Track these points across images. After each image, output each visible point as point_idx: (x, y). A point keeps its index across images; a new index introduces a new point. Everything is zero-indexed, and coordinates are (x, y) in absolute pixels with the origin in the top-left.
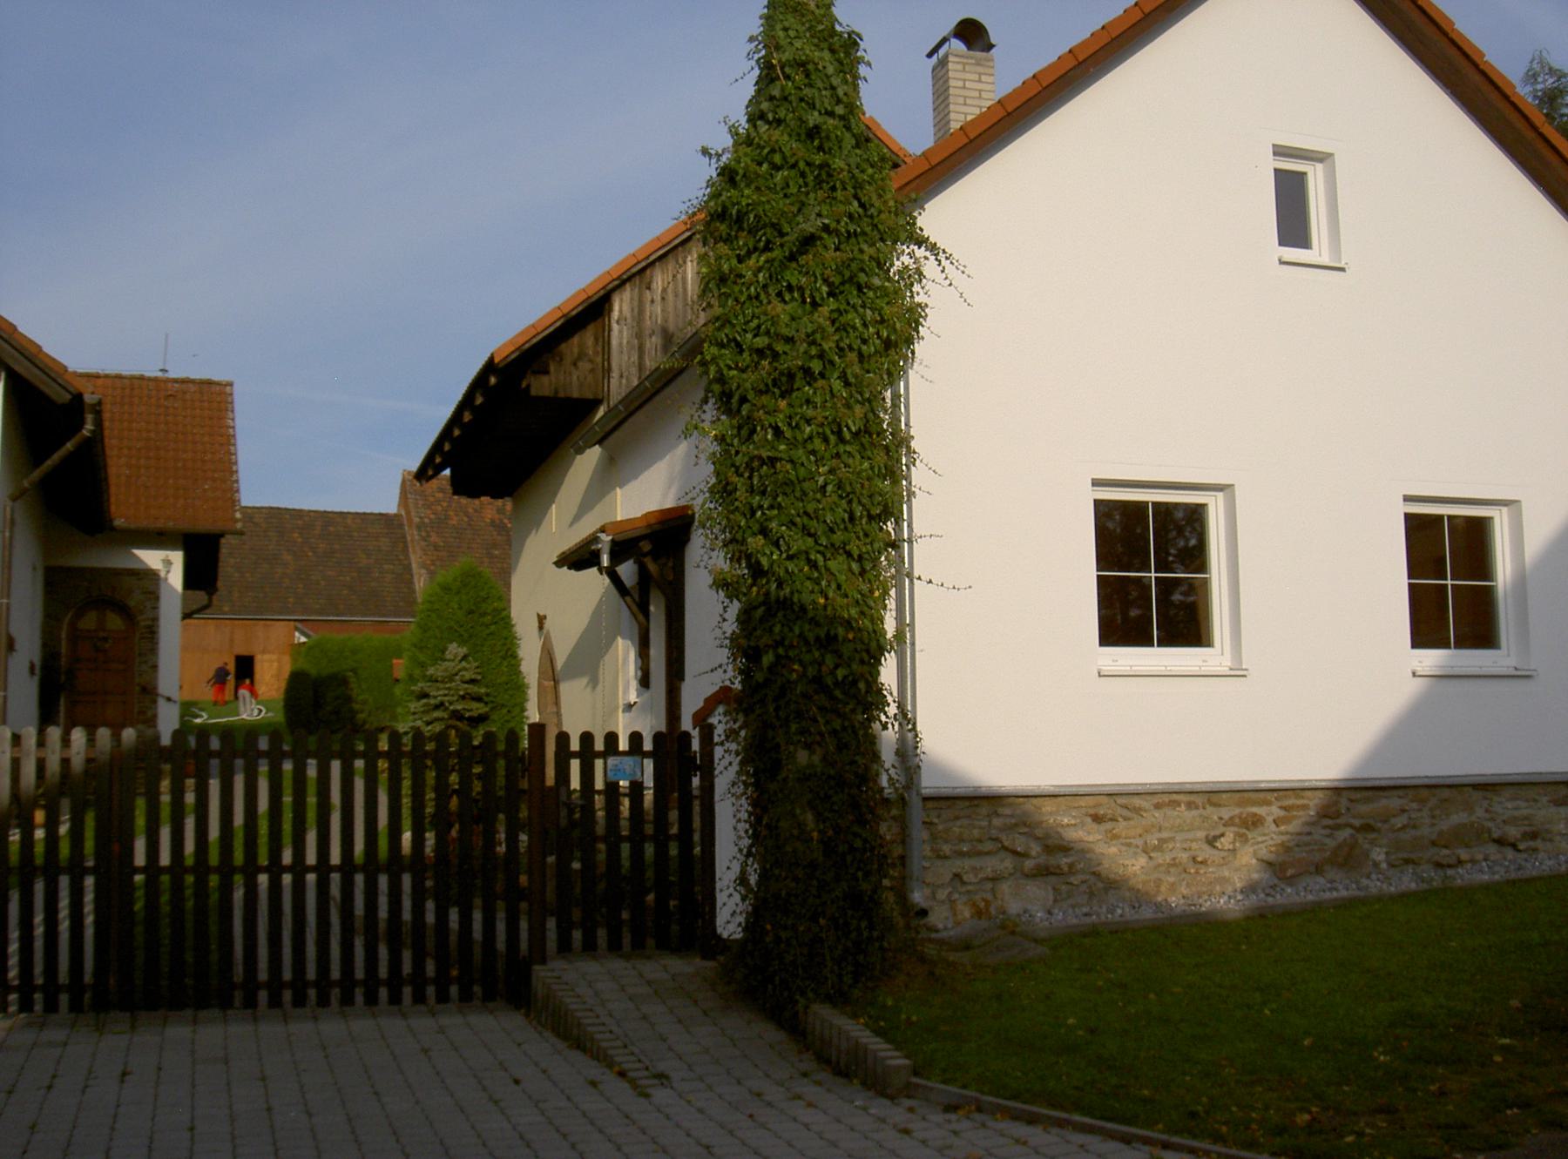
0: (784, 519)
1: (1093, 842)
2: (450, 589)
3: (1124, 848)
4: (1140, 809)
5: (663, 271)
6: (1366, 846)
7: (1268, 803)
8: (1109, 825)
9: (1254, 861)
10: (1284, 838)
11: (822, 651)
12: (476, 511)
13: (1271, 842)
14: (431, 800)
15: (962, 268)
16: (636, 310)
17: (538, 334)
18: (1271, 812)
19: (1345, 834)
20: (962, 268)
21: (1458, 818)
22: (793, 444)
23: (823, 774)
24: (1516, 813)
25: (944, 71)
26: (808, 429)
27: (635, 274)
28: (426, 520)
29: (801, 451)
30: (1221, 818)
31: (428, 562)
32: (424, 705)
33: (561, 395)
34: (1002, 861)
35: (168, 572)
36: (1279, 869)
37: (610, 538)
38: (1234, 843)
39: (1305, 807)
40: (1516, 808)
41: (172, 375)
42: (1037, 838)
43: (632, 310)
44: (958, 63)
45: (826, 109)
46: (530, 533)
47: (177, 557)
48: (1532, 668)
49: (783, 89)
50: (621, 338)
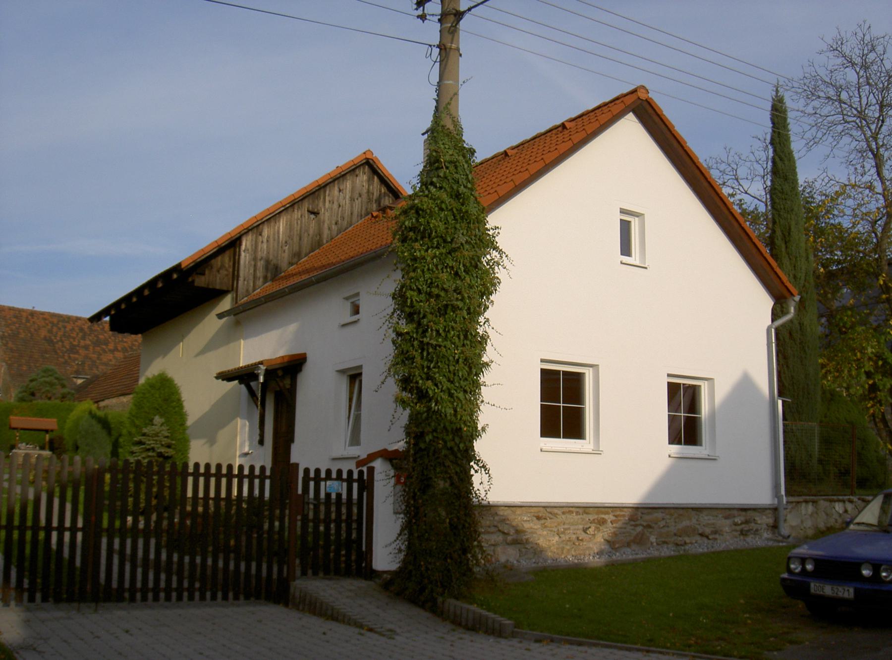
1: (536, 529)
3: (549, 532)
4: (557, 514)
7: (607, 513)
8: (543, 521)
9: (603, 540)
10: (615, 530)
13: (609, 532)
16: (254, 245)
18: (609, 517)
19: (640, 529)
21: (686, 523)
22: (446, 339)
24: (710, 522)
26: (452, 333)
27: (254, 227)
28: (6, 334)
29: (449, 342)
30: (589, 520)
31: (7, 359)
32: (140, 449)
33: (211, 287)
34: (498, 536)
37: (265, 368)
39: (624, 516)
40: (709, 520)
43: (252, 245)
48: (717, 455)
49: (445, 173)
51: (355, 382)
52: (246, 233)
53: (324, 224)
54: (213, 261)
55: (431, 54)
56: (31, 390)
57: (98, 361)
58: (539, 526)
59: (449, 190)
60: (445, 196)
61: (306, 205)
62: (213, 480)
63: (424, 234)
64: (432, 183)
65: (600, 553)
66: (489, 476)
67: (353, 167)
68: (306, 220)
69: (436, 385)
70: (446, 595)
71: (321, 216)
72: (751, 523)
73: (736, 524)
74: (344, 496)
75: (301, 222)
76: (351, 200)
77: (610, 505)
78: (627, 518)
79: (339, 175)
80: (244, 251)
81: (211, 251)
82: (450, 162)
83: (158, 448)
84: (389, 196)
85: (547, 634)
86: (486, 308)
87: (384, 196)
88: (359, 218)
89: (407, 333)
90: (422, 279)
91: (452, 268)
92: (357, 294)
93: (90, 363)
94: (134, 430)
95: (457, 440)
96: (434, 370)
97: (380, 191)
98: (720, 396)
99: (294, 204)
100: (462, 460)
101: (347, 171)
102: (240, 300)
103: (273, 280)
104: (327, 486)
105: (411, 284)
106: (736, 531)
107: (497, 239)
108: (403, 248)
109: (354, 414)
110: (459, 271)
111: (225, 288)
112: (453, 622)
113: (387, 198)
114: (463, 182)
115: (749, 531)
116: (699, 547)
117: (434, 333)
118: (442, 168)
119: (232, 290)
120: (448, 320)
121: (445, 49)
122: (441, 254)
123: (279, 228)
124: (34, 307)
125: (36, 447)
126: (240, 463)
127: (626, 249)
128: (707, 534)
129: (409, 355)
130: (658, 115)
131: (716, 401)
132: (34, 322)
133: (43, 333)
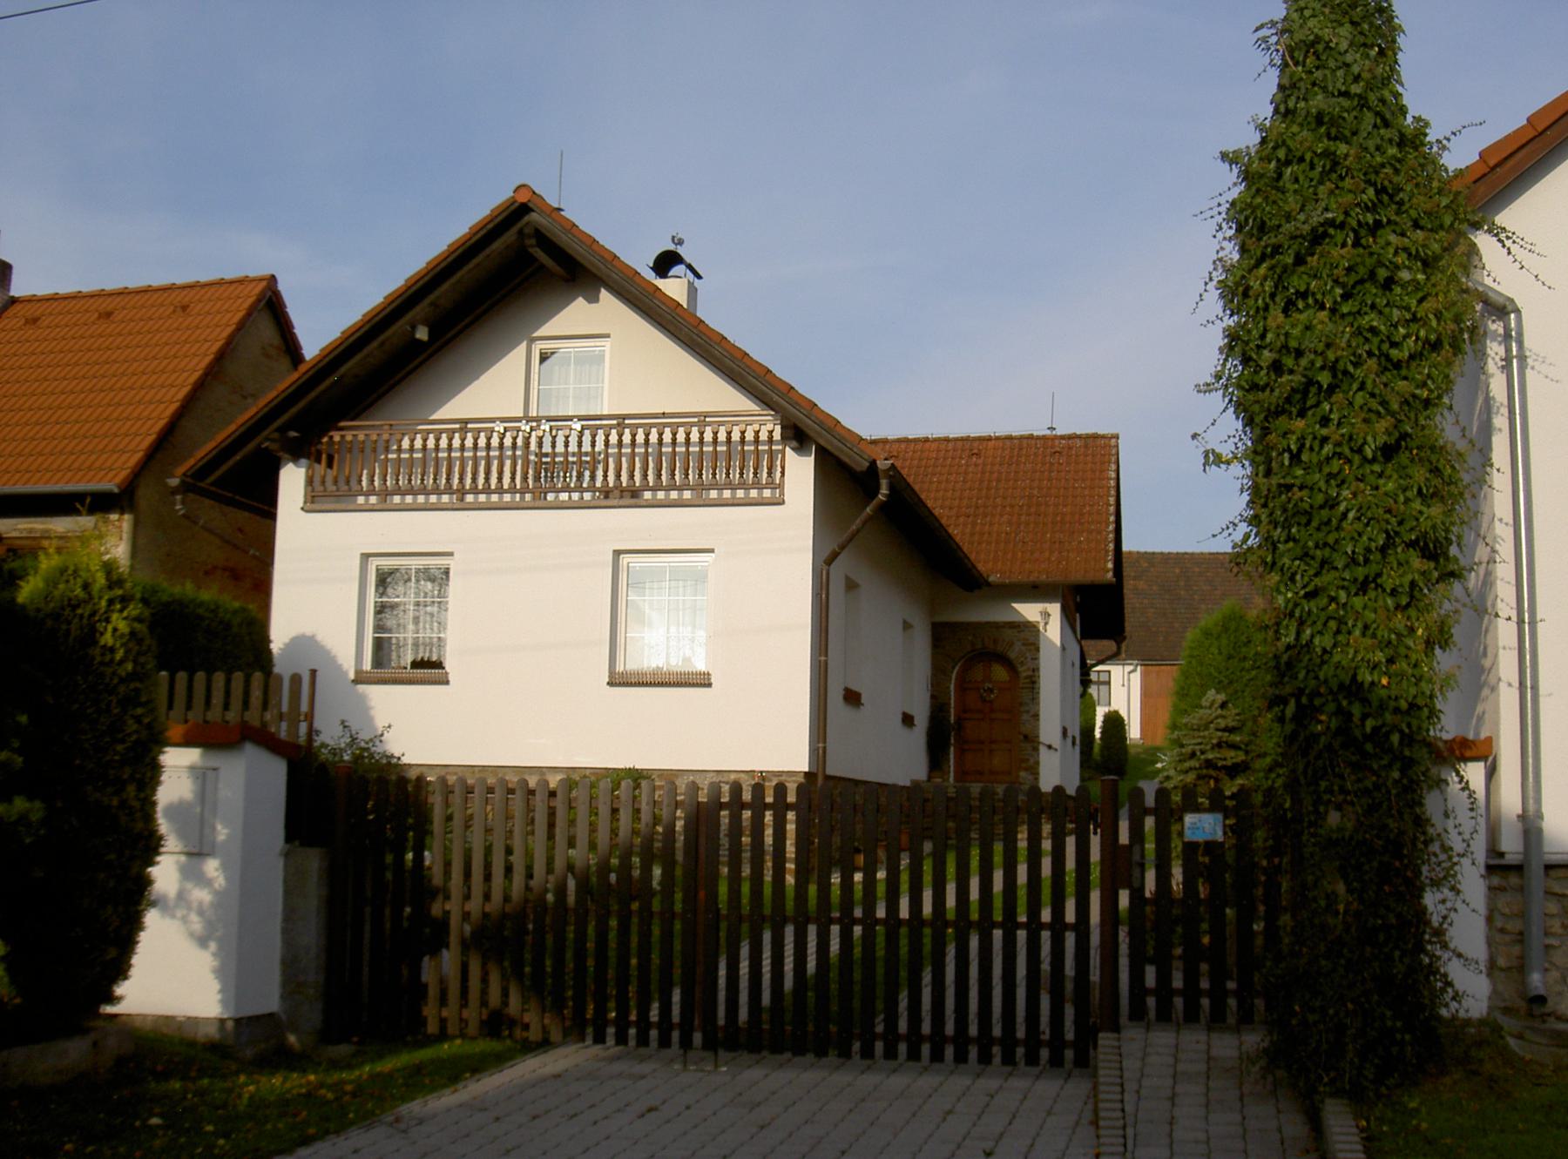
0: (1299, 552)
2: (1211, 634)
14: (746, 851)
15: (1529, 247)
20: (1529, 247)
35: (1046, 624)
41: (1059, 432)
45: (1339, 91)
47: (1055, 609)
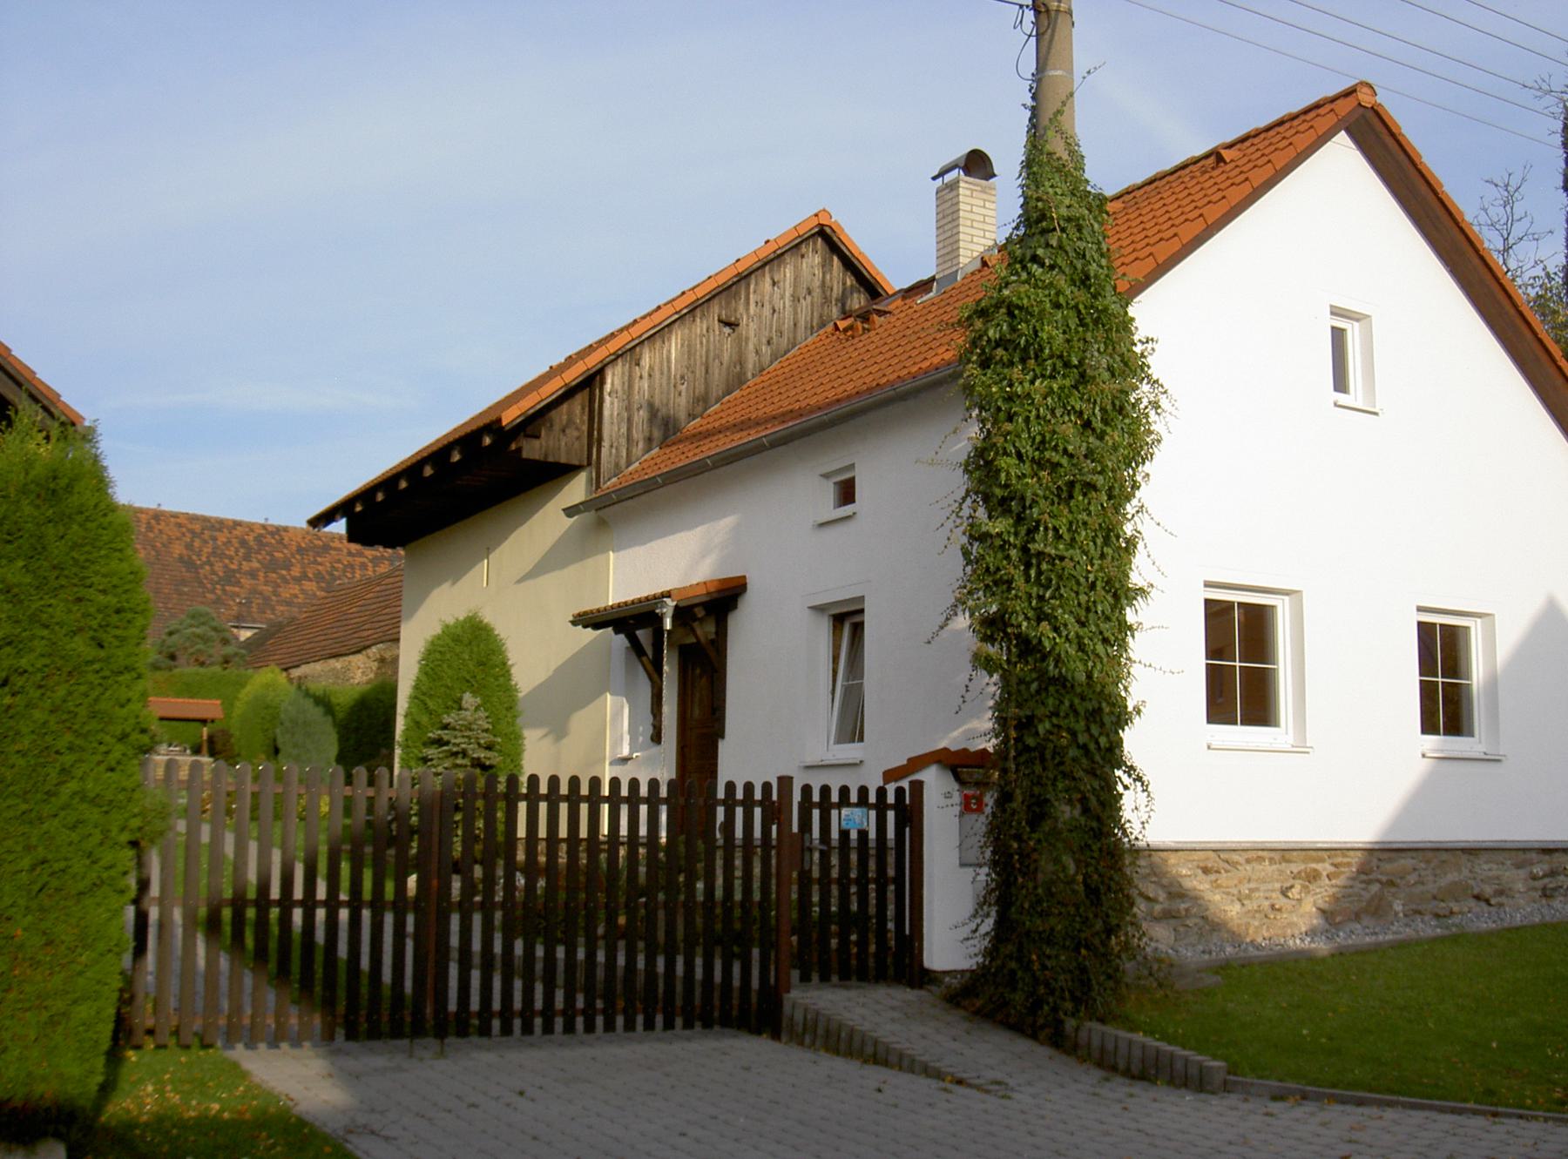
3: (1224, 896)
5: (650, 351)
6: (1390, 898)
7: (1322, 860)
8: (1213, 877)
9: (1314, 909)
10: (1334, 890)
11: (1036, 721)
12: (164, 545)
13: (1325, 894)
17: (542, 400)
18: (1325, 868)
19: (1375, 888)
21: (1452, 876)
22: (1072, 543)
23: (1086, 826)
24: (1490, 874)
25: (954, 193)
29: (1078, 551)
30: (1292, 872)
33: (551, 459)
36: (1330, 917)
37: (675, 603)
38: (1300, 893)
39: (1349, 864)
40: (1490, 870)
42: (1163, 887)
43: (624, 383)
44: (967, 189)
46: (446, 581)
49: (1060, 239)
50: (612, 410)
51: (842, 630)
52: (612, 361)
53: (747, 343)
54: (554, 414)
55: (1021, 22)
56: (172, 650)
57: (274, 598)
58: (1207, 886)
59: (1067, 270)
60: (1062, 282)
61: (716, 309)
62: (564, 808)
63: (1029, 353)
64: (1035, 259)
65: (1312, 933)
66: (1149, 796)
67: (797, 242)
68: (717, 338)
69: (1056, 629)
70: (1082, 1014)
71: (742, 329)
72: (1559, 874)
73: (1535, 878)
74: (872, 835)
75: (708, 341)
76: (793, 301)
77: (1325, 846)
78: (1354, 870)
79: (772, 256)
80: (610, 394)
81: (553, 393)
82: (1069, 220)
83: (473, 750)
84: (859, 292)
85: (1292, 1085)
86: (1136, 486)
87: (852, 293)
88: (809, 332)
89: (999, 535)
90: (1024, 435)
91: (1080, 414)
92: (852, 466)
93: (260, 601)
94: (425, 719)
95: (1095, 730)
96: (1052, 601)
97: (844, 284)
98: (1504, 649)
99: (696, 307)
100: (1103, 767)
101: (787, 248)
102: (605, 483)
103: (663, 444)
104: (843, 817)
105: (1006, 445)
106: (1535, 889)
107: (1150, 360)
108: (984, 379)
109: (842, 686)
110: (1093, 419)
111: (575, 462)
112: (1100, 1064)
113: (855, 295)
114: (1092, 256)
115: (1555, 889)
116: (1482, 921)
117: (1051, 534)
118: (1054, 229)
119: (589, 464)
120: (1074, 509)
121: (1048, 11)
122: (1061, 388)
123: (669, 351)
124: (159, 505)
125: (185, 750)
126: (613, 775)
127: (1341, 384)
128: (1487, 896)
129: (1001, 577)
130: (1393, 135)
131: (1498, 659)
132: (161, 531)
133: (178, 549)
